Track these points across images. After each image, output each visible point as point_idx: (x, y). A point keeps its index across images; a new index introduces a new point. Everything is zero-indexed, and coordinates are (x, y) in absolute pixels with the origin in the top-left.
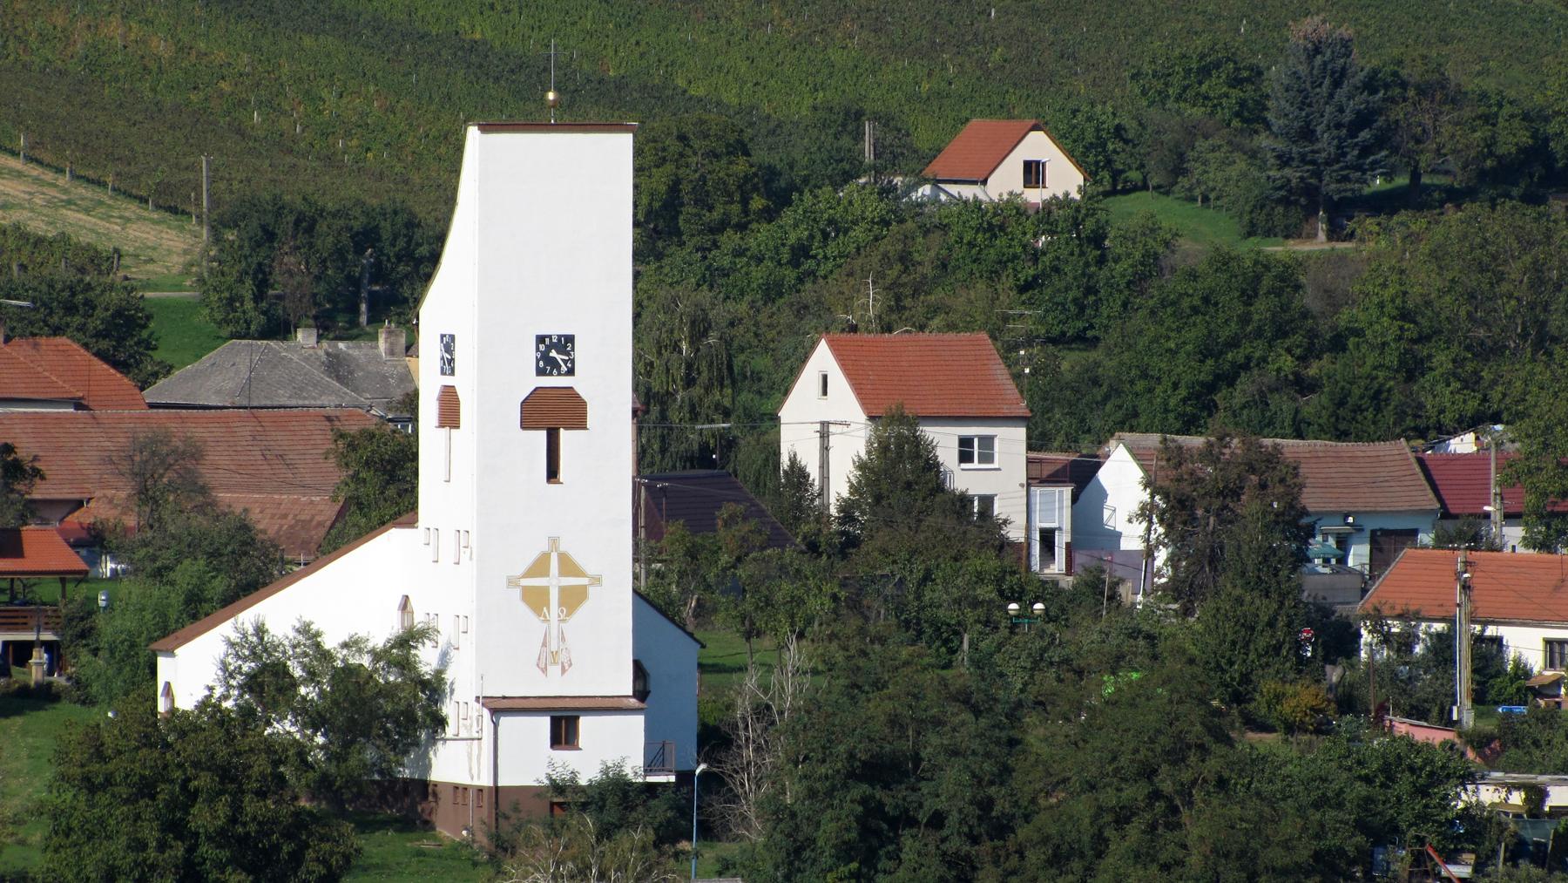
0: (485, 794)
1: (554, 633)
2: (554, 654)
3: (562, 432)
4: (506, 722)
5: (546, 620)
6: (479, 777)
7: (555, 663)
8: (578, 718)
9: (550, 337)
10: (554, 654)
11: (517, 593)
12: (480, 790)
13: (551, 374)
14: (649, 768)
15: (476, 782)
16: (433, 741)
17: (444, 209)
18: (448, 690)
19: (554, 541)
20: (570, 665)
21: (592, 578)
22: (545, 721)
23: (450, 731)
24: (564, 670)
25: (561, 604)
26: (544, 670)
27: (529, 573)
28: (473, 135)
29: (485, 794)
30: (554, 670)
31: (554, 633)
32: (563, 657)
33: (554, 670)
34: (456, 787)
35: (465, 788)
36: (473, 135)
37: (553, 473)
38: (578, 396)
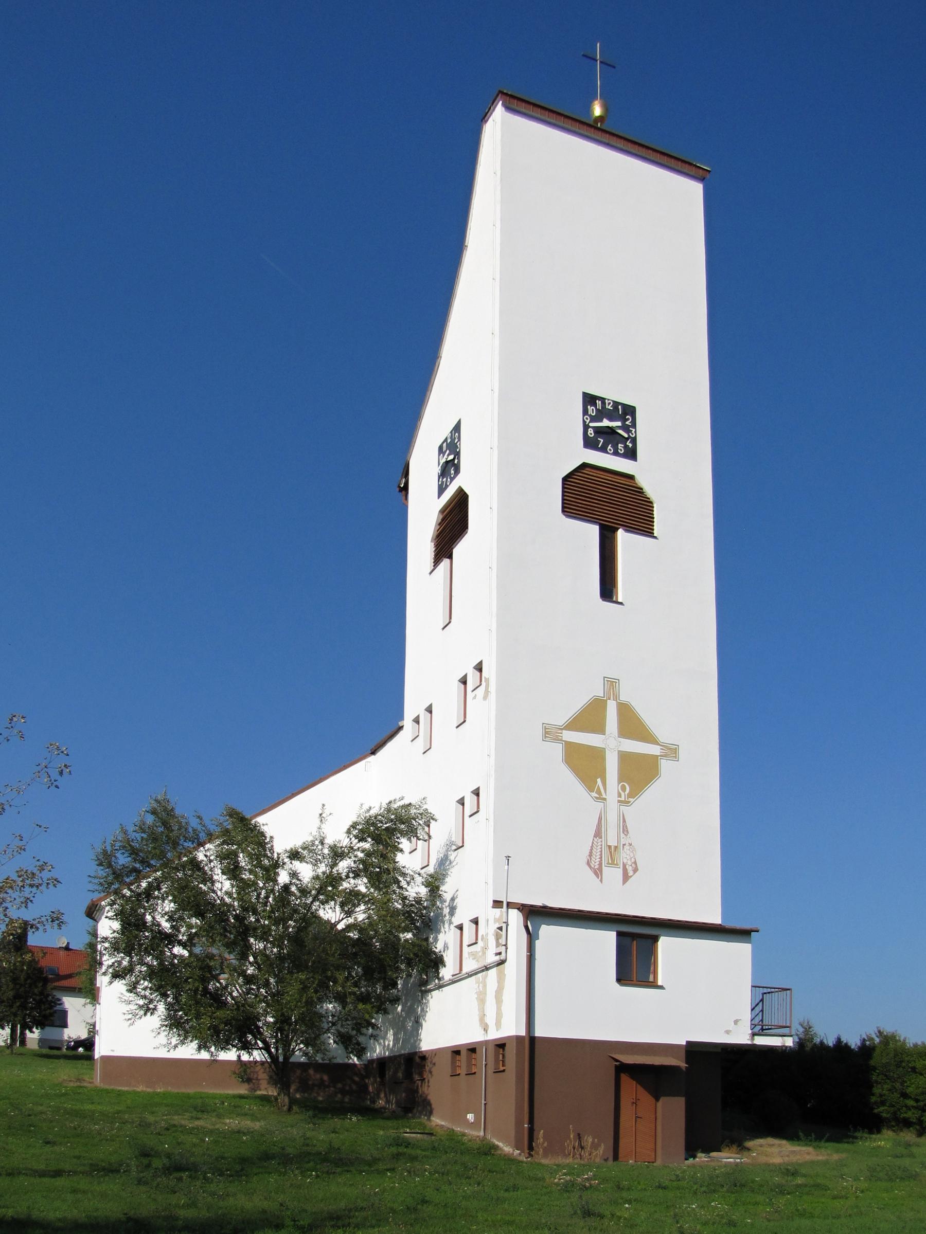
0: (511, 1052)
1: (612, 818)
2: (613, 851)
3: (621, 533)
4: (548, 932)
5: (601, 799)
6: (498, 1024)
7: (613, 863)
8: (655, 939)
9: (603, 400)
10: (613, 851)
11: (557, 750)
12: (501, 1045)
13: (604, 450)
14: (760, 1028)
15: (494, 1034)
16: (422, 989)
17: (405, 502)
18: (446, 911)
19: (611, 684)
20: (635, 870)
21: (664, 746)
22: (608, 939)
23: (446, 973)
24: (626, 878)
25: (621, 779)
26: (598, 873)
27: (575, 724)
28: (499, 111)
29: (511, 1052)
30: (613, 874)
31: (612, 818)
32: (624, 856)
33: (613, 874)
34: (456, 1052)
35: (472, 1049)
36: (499, 111)
37: (608, 590)
38: (640, 491)
